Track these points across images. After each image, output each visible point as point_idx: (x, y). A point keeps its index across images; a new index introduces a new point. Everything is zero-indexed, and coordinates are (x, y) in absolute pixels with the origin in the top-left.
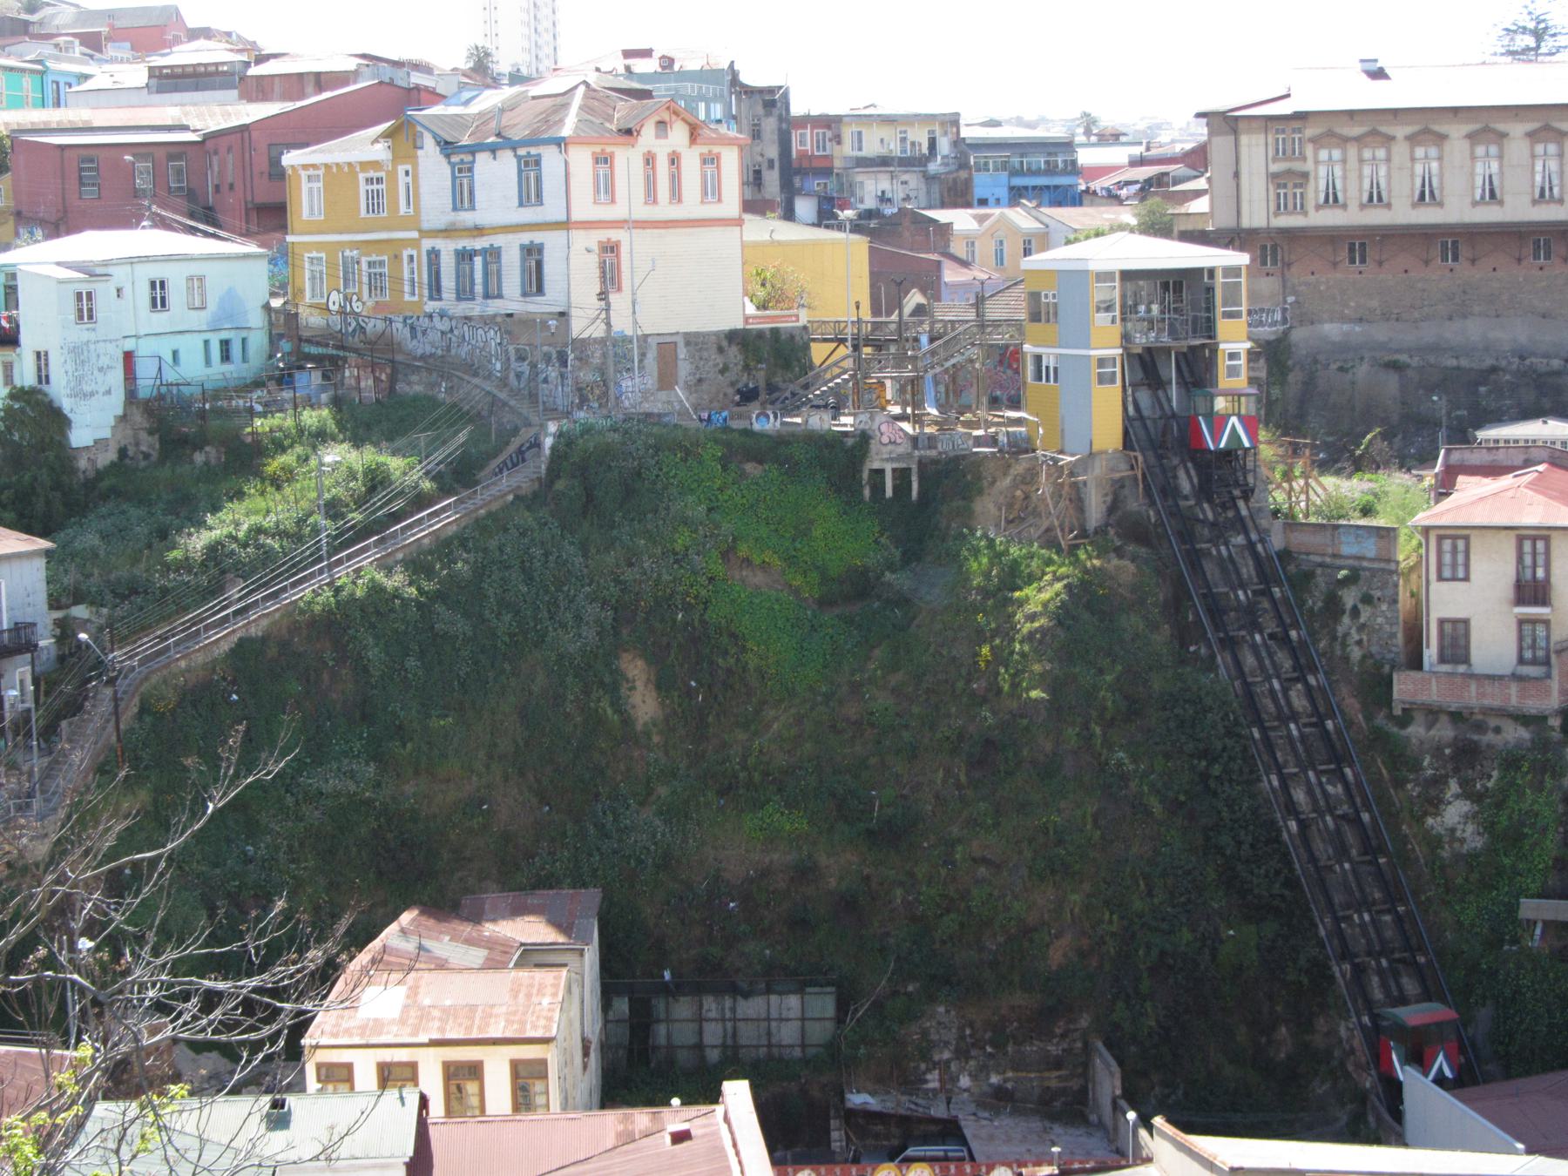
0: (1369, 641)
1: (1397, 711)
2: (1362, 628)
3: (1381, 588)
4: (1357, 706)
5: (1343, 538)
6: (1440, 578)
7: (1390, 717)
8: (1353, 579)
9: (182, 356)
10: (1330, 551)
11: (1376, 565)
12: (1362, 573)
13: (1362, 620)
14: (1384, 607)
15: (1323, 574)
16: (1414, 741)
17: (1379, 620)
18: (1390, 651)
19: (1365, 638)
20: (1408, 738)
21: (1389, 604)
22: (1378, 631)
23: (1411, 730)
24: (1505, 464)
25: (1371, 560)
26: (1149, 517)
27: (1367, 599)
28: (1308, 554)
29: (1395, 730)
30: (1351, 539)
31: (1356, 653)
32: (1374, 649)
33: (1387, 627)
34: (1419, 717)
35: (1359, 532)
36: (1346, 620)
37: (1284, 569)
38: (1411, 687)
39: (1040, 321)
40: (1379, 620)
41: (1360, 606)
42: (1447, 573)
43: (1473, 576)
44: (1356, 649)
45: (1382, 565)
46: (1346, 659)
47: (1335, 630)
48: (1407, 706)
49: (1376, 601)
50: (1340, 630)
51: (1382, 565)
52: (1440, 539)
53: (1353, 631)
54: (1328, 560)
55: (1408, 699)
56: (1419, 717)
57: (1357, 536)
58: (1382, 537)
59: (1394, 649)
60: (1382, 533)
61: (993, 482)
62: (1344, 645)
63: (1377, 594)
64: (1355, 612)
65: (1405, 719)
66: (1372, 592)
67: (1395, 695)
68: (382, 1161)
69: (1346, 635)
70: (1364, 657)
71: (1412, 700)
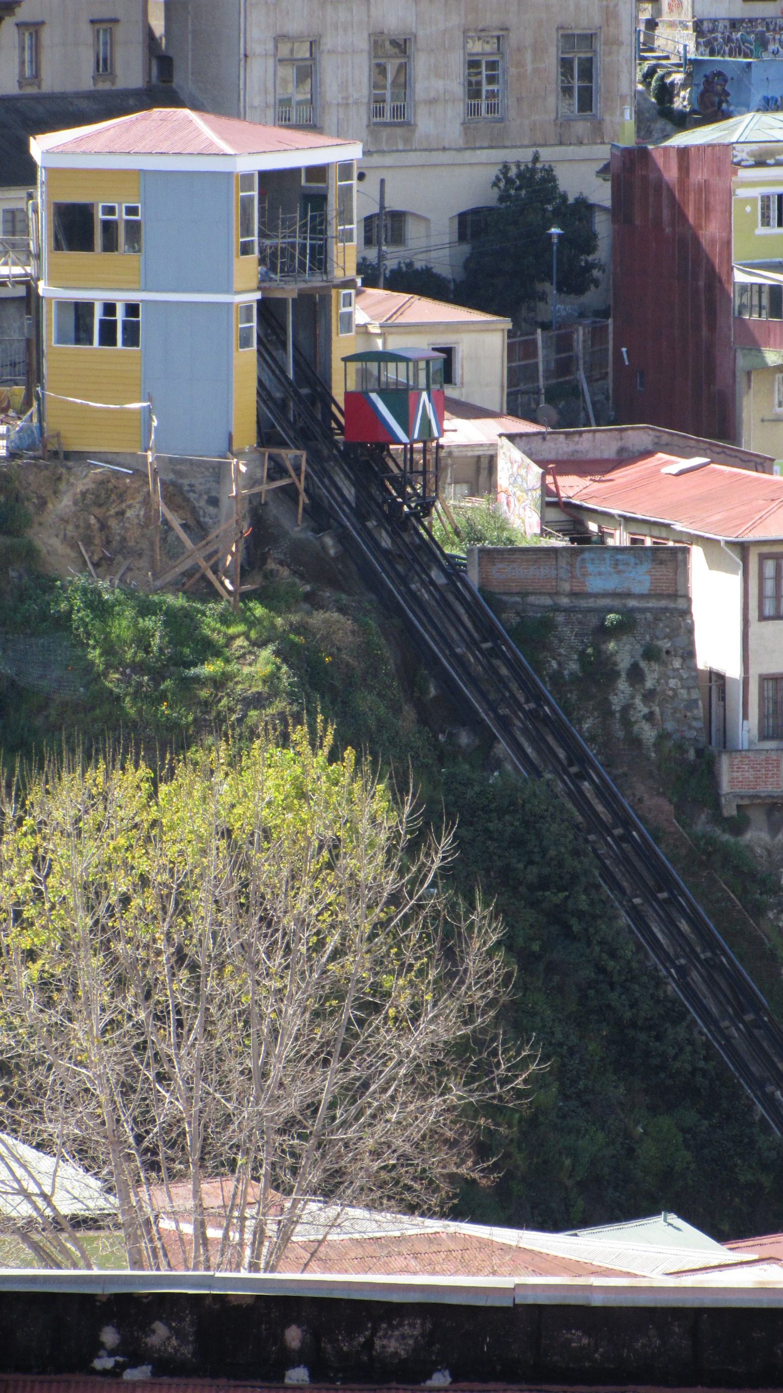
0: (662, 714)
1: (730, 811)
2: (649, 696)
3: (668, 637)
4: (668, 808)
5: (590, 568)
6: (762, 618)
7: (718, 818)
8: (626, 627)
9: (461, 368)
10: (566, 587)
11: (652, 604)
12: (638, 616)
13: (649, 684)
14: (677, 663)
15: (567, 623)
16: (758, 850)
17: (673, 683)
18: (690, 727)
19: (657, 710)
20: (749, 848)
21: (683, 657)
22: (673, 698)
23: (749, 836)
24: (591, 456)
25: (641, 597)
26: (324, 547)
27: (651, 654)
28: (525, 594)
29: (726, 837)
30: (606, 568)
31: (648, 733)
32: (670, 726)
33: (683, 692)
34: (758, 817)
35: (620, 557)
36: (623, 685)
37: (500, 620)
38: (749, 774)
39: (86, 245)
40: (673, 683)
41: (643, 664)
42: (769, 610)
43: (764, 623)
44: (646, 726)
45: (663, 603)
46: (636, 742)
47: (606, 703)
48: (746, 802)
49: (664, 655)
50: (617, 702)
51: (663, 603)
52: (763, 558)
53: (638, 701)
54: (565, 601)
55: (745, 791)
56: (758, 817)
57: (616, 563)
58: (661, 562)
59: (694, 724)
60: (663, 556)
61: (214, 502)
62: (627, 724)
63: (665, 644)
64: (636, 674)
65: (738, 826)
66: (660, 643)
67: (725, 787)
68: (638, 864)
69: (627, 708)
70: (663, 736)
71: (752, 792)
